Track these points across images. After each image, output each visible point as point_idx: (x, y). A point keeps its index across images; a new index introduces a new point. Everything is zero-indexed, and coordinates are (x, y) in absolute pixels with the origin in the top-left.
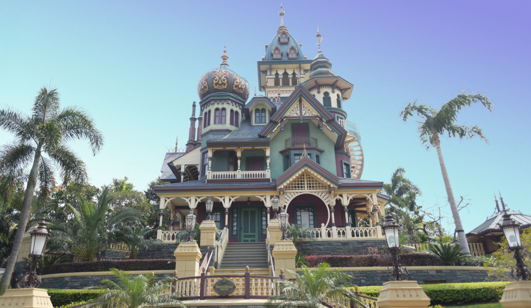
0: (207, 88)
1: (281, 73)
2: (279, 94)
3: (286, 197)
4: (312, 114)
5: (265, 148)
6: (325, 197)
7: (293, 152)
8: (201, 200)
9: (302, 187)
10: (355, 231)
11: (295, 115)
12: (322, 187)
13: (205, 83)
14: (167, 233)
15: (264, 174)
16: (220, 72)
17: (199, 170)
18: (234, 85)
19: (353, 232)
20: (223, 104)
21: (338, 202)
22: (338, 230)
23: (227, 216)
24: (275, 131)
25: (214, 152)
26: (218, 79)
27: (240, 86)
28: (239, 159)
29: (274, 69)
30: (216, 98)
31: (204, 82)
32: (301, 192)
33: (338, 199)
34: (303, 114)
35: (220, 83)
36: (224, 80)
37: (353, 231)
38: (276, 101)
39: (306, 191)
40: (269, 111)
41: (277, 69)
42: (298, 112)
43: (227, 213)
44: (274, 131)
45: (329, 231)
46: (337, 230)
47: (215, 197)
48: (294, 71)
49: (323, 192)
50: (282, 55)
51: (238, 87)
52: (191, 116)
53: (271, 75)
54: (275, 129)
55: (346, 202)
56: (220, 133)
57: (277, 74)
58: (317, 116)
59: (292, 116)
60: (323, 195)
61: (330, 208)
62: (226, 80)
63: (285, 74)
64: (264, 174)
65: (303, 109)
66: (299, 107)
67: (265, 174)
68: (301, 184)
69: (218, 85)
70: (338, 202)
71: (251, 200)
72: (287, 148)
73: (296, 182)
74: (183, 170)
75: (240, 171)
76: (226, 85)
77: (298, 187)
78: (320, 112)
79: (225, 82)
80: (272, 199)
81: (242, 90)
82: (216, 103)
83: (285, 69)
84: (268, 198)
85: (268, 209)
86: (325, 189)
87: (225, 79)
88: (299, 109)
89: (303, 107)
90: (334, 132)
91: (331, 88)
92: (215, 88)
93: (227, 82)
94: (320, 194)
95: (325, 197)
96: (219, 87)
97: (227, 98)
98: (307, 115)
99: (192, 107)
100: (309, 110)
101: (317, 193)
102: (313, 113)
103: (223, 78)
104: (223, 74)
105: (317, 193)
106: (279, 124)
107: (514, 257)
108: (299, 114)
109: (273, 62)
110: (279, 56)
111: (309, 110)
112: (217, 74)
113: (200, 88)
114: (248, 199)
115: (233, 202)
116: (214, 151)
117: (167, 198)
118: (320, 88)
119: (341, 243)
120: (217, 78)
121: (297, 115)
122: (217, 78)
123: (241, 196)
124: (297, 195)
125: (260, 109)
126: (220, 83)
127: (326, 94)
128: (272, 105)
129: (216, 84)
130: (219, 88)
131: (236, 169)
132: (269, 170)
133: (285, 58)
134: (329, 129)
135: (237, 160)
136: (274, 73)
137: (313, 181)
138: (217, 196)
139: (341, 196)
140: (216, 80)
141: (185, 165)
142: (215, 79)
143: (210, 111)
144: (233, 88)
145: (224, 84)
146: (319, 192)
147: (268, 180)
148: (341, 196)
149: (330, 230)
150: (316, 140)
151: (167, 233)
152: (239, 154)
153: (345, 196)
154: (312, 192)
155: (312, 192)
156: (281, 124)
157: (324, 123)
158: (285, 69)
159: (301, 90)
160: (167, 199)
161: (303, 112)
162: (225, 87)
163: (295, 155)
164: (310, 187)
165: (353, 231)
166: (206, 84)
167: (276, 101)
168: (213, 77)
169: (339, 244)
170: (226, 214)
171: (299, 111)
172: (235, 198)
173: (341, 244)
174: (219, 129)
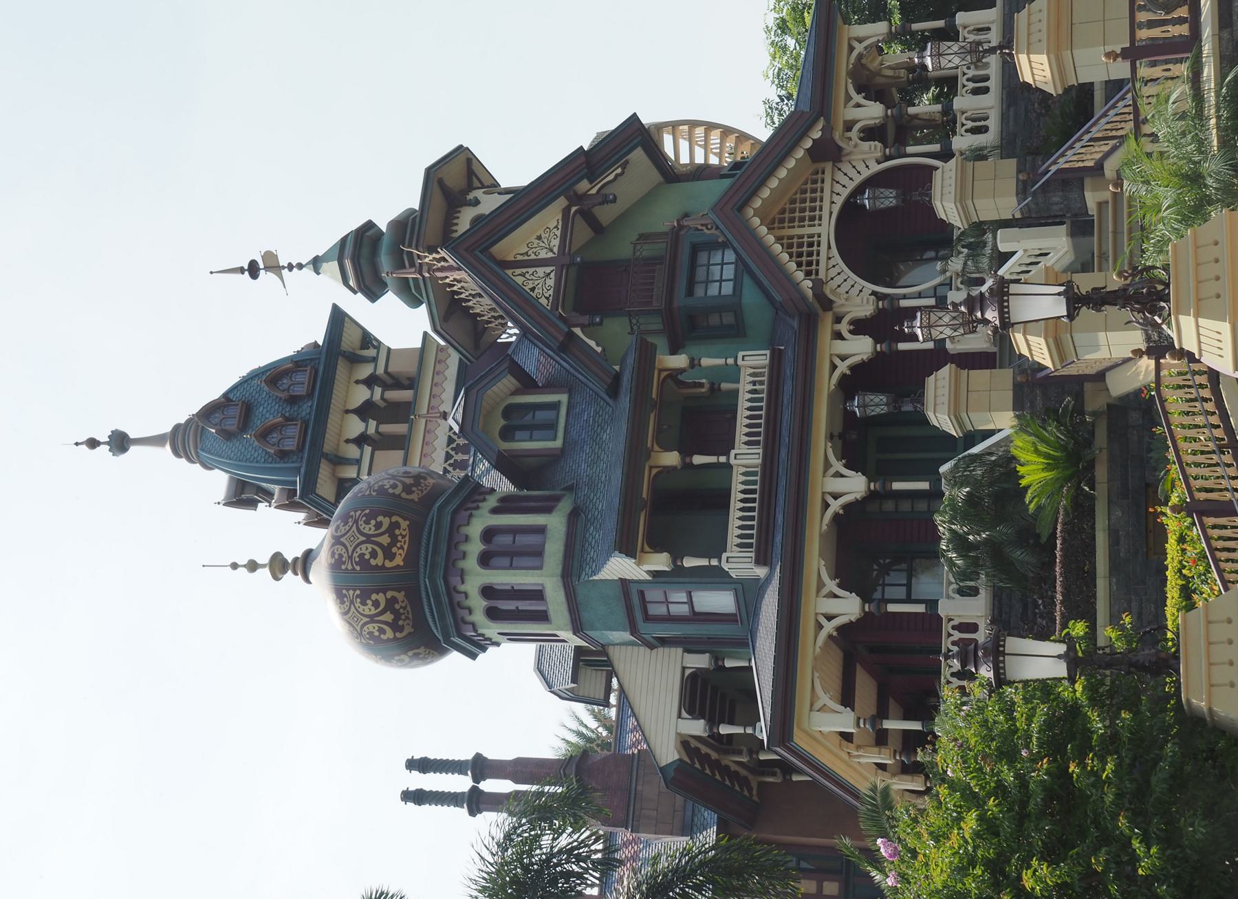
1: (355, 427)
3: (842, 290)
4: (556, 227)
5: (661, 371)
6: (852, 173)
7: (680, 298)
8: (833, 578)
9: (811, 245)
10: (970, 124)
11: (551, 282)
12: (815, 182)
13: (376, 604)
14: (950, 635)
15: (744, 474)
16: (343, 540)
17: (701, 661)
18: (404, 495)
19: (976, 92)
20: (467, 539)
21: (870, 134)
22: (964, 133)
23: (897, 486)
24: (598, 345)
25: (650, 546)
26: (369, 546)
27: (409, 481)
28: (688, 460)
30: (441, 560)
31: (369, 609)
32: (829, 247)
33: (852, 327)
34: (550, 255)
35: (389, 540)
36: (378, 526)
37: (967, 131)
38: (466, 457)
39: (826, 229)
40: (516, 393)
41: (339, 441)
42: (541, 271)
43: (884, 486)
44: (599, 349)
45: (954, 628)
47: (833, 387)
48: (357, 382)
49: (833, 180)
50: (289, 419)
51: (412, 485)
52: (464, 811)
53: (358, 462)
54: (592, 343)
55: (873, 112)
56: (578, 547)
57: (361, 440)
58: (566, 211)
59: (551, 292)
60: (845, 180)
61: (887, 158)
62: (374, 597)
63: (365, 411)
64: (744, 474)
66: (524, 270)
67: (745, 470)
68: (800, 245)
69: (394, 550)
70: (870, 134)
71: (838, 429)
72: (661, 327)
73: (800, 212)
74: (697, 727)
76: (400, 520)
77: (810, 254)
78: (556, 193)
79: (386, 522)
80: (846, 334)
81: (393, 600)
82: (462, 564)
83: (347, 412)
84: (841, 347)
85: (867, 609)
86: (823, 173)
87: (373, 522)
88: (531, 270)
89: (526, 258)
90: (627, 162)
92: (402, 564)
93: (385, 514)
94: (838, 188)
95: (852, 173)
96: (402, 548)
97: (447, 519)
98: (556, 243)
99: (426, 808)
100: (539, 238)
101: (836, 198)
102: (552, 224)
103: (369, 529)
104: (354, 528)
105: (836, 198)
106: (578, 331)
107: (1099, 310)
108: (548, 270)
109: (313, 444)
110: (293, 431)
111: (539, 238)
112: (350, 550)
114: (836, 439)
115: (846, 466)
116: (647, 548)
117: (818, 591)
119: (1008, 107)
120: (366, 549)
121: (552, 275)
122: (366, 549)
123: (820, 555)
124: (837, 259)
125: (502, 422)
126: (389, 540)
128: (502, 368)
129: (389, 556)
130: (406, 547)
132: (741, 354)
133: (306, 409)
134: (617, 176)
135: (691, 465)
136: (352, 451)
137: (793, 211)
138: (826, 384)
139: (849, 126)
140: (374, 554)
141: (679, 716)
144: (398, 566)
145: (395, 525)
146: (832, 192)
147: (777, 359)
148: (849, 126)
149: (952, 623)
150: (644, 237)
151: (950, 635)
152: (671, 459)
153: (851, 113)
154: (831, 213)
155: (831, 213)
156: (576, 326)
157: (594, 191)
158: (347, 412)
159: (466, 250)
161: (544, 254)
162: (404, 524)
163: (690, 292)
164: (811, 245)
165: (967, 131)
166: (381, 598)
167: (466, 457)
168: (358, 568)
169: (1011, 113)
170: (888, 488)
171: (538, 269)
173: (1012, 109)
174: (562, 548)
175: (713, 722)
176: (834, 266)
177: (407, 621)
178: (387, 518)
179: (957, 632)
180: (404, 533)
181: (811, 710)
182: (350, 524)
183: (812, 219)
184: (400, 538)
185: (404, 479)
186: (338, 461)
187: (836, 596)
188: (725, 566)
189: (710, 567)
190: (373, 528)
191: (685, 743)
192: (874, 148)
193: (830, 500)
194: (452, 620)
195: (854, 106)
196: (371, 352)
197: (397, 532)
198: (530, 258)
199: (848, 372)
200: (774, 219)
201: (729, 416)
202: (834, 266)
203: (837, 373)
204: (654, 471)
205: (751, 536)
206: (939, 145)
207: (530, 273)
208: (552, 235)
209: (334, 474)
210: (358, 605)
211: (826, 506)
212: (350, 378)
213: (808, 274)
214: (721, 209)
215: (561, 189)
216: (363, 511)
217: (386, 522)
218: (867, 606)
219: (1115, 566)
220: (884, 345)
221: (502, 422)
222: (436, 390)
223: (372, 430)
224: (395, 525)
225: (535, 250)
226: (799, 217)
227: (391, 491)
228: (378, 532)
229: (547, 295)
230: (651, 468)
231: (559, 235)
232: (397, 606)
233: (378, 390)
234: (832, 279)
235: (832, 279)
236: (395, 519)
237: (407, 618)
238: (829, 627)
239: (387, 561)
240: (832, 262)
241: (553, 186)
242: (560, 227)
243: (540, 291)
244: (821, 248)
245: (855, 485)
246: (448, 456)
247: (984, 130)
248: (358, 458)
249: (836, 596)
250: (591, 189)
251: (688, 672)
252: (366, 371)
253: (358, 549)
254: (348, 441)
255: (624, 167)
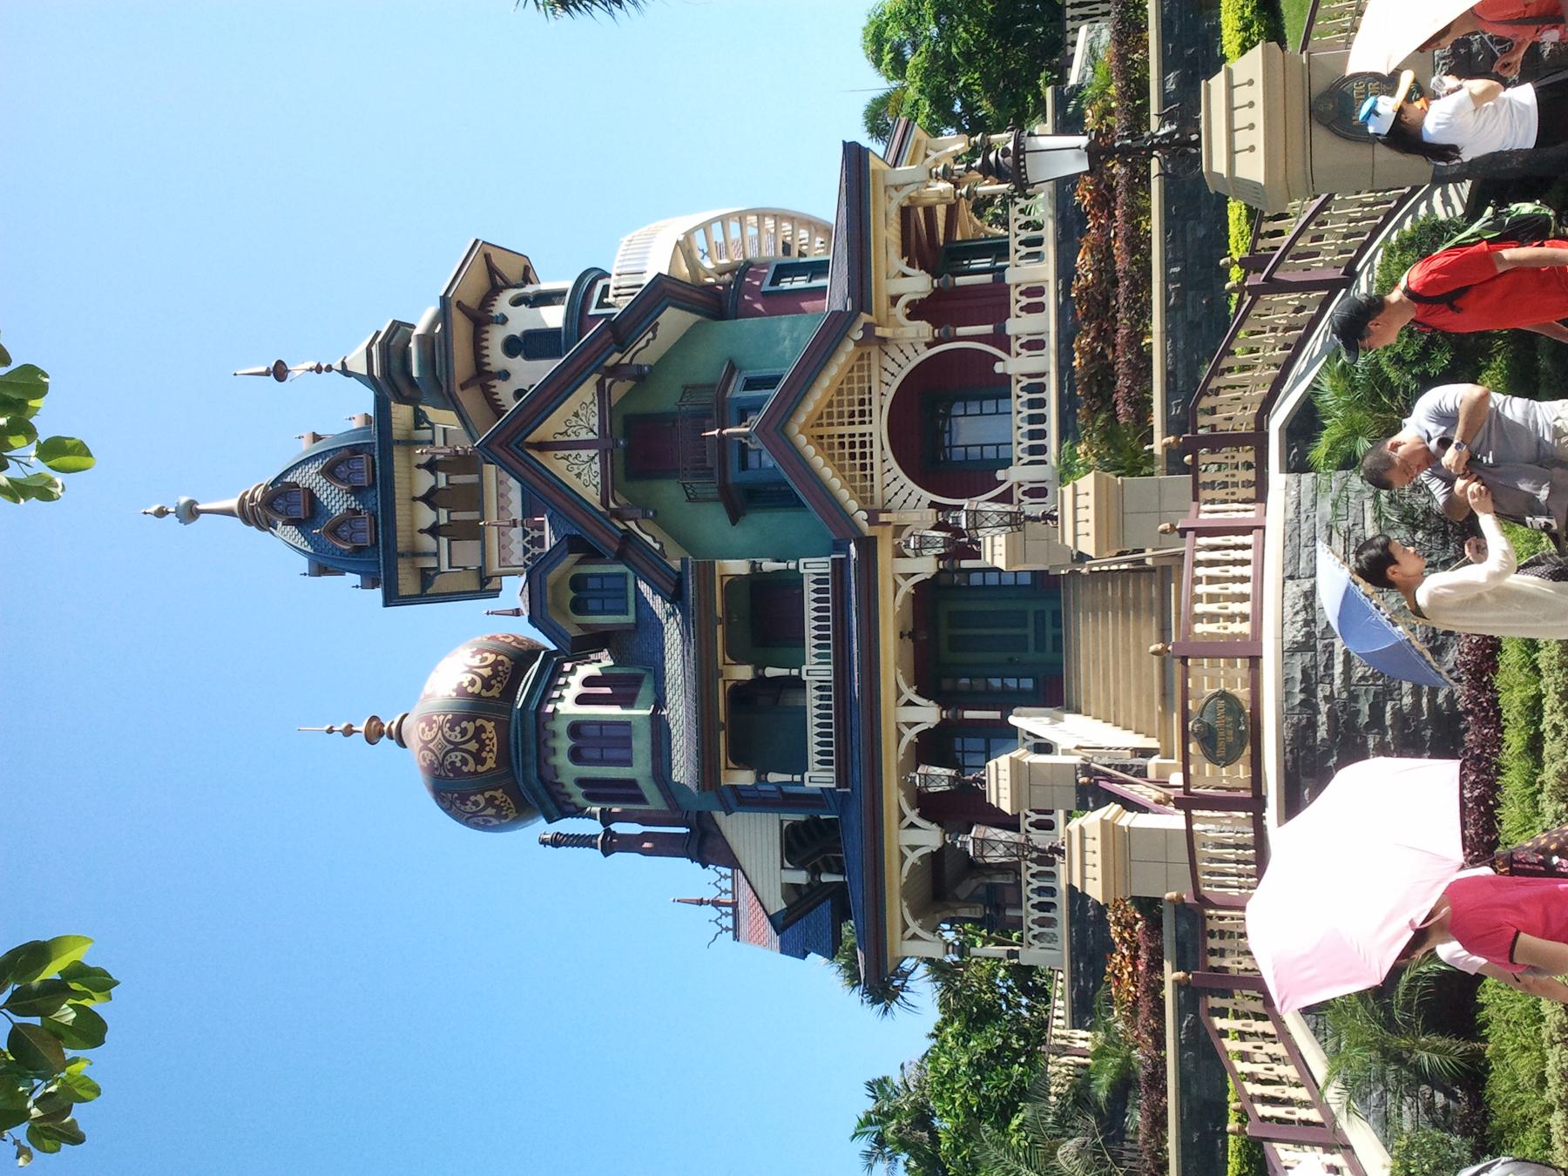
0: (492, 793)
1: (426, 516)
2: (514, 523)
4: (592, 402)
6: (901, 359)
9: (863, 444)
10: (1025, 301)
11: (596, 467)
12: (861, 368)
13: (476, 803)
14: (1029, 883)
18: (484, 693)
20: (554, 735)
21: (917, 310)
22: (1020, 351)
29: (413, 543)
34: (591, 436)
35: (477, 746)
36: (464, 732)
37: (1022, 309)
39: (878, 428)
41: (412, 531)
44: (657, 546)
46: (1017, 316)
47: (901, 757)
48: (419, 466)
53: (436, 555)
54: (649, 539)
57: (435, 531)
59: (598, 479)
63: (432, 498)
65: (573, 438)
67: (816, 577)
68: (852, 445)
69: (484, 754)
70: (917, 310)
72: (717, 496)
74: (801, 877)
75: (804, 668)
76: (485, 723)
77: (863, 456)
79: (471, 727)
82: (553, 760)
83: (415, 499)
85: (941, 566)
88: (574, 453)
89: (566, 438)
90: (657, 324)
91: (487, 328)
92: (498, 696)
94: (887, 377)
95: (901, 359)
96: (491, 751)
98: (595, 421)
100: (576, 415)
102: (588, 400)
108: (592, 453)
113: (495, 822)
116: (731, 764)
118: (487, 368)
121: (597, 459)
125: (572, 594)
126: (477, 746)
127: (513, 346)
129: (480, 761)
131: (798, 684)
134: (648, 341)
136: (428, 542)
138: (893, 754)
140: (464, 762)
141: (783, 867)
142: (458, 764)
143: (581, 782)
145: (480, 730)
149: (1020, 342)
152: (744, 673)
158: (415, 499)
159: (500, 445)
160: (909, 933)
161: (585, 435)
162: (490, 726)
168: (451, 775)
172: (909, 920)
174: (649, 746)
175: (815, 872)
176: (889, 471)
177: (499, 685)
178: (471, 723)
179: (1036, 911)
180: (491, 736)
181: (902, 939)
182: (435, 730)
183: (862, 413)
184: (487, 742)
185: (480, 671)
186: (415, 554)
187: (904, 275)
188: (804, 677)
189: (790, 677)
190: (459, 736)
191: (790, 889)
192: (923, 329)
193: (904, 730)
194: (560, 499)
195: (906, 705)
196: (427, 434)
197: (484, 736)
198: (570, 439)
199: (917, 810)
200: (822, 413)
201: (797, 592)
202: (889, 471)
203: (905, 742)
204: (729, 684)
205: (827, 637)
206: (991, 327)
207: (574, 456)
208: (589, 411)
209: (413, 567)
210: (458, 805)
211: (900, 735)
212: (410, 462)
213: (863, 500)
214: (763, 430)
215: (593, 367)
216: (446, 716)
217: (471, 727)
218: (944, 713)
219: (1168, 311)
220: (950, 713)
221: (572, 594)
222: (502, 489)
223: (442, 484)
224: (480, 730)
225: (575, 429)
226: (844, 465)
227: (470, 690)
228: (466, 738)
229: (595, 483)
230: (725, 681)
231: (597, 412)
232: (497, 802)
233: (442, 476)
234: (888, 485)
235: (888, 485)
236: (479, 722)
237: (501, 682)
238: (910, 735)
239: (479, 766)
240: (887, 466)
241: (581, 366)
242: (596, 402)
243: (587, 478)
244: (874, 472)
245: (930, 837)
246: (526, 550)
247: (1040, 308)
248: (436, 551)
249: (904, 275)
250: (622, 358)
251: (785, 824)
252: (421, 454)
253: (448, 757)
254: (421, 531)
255: (654, 330)
